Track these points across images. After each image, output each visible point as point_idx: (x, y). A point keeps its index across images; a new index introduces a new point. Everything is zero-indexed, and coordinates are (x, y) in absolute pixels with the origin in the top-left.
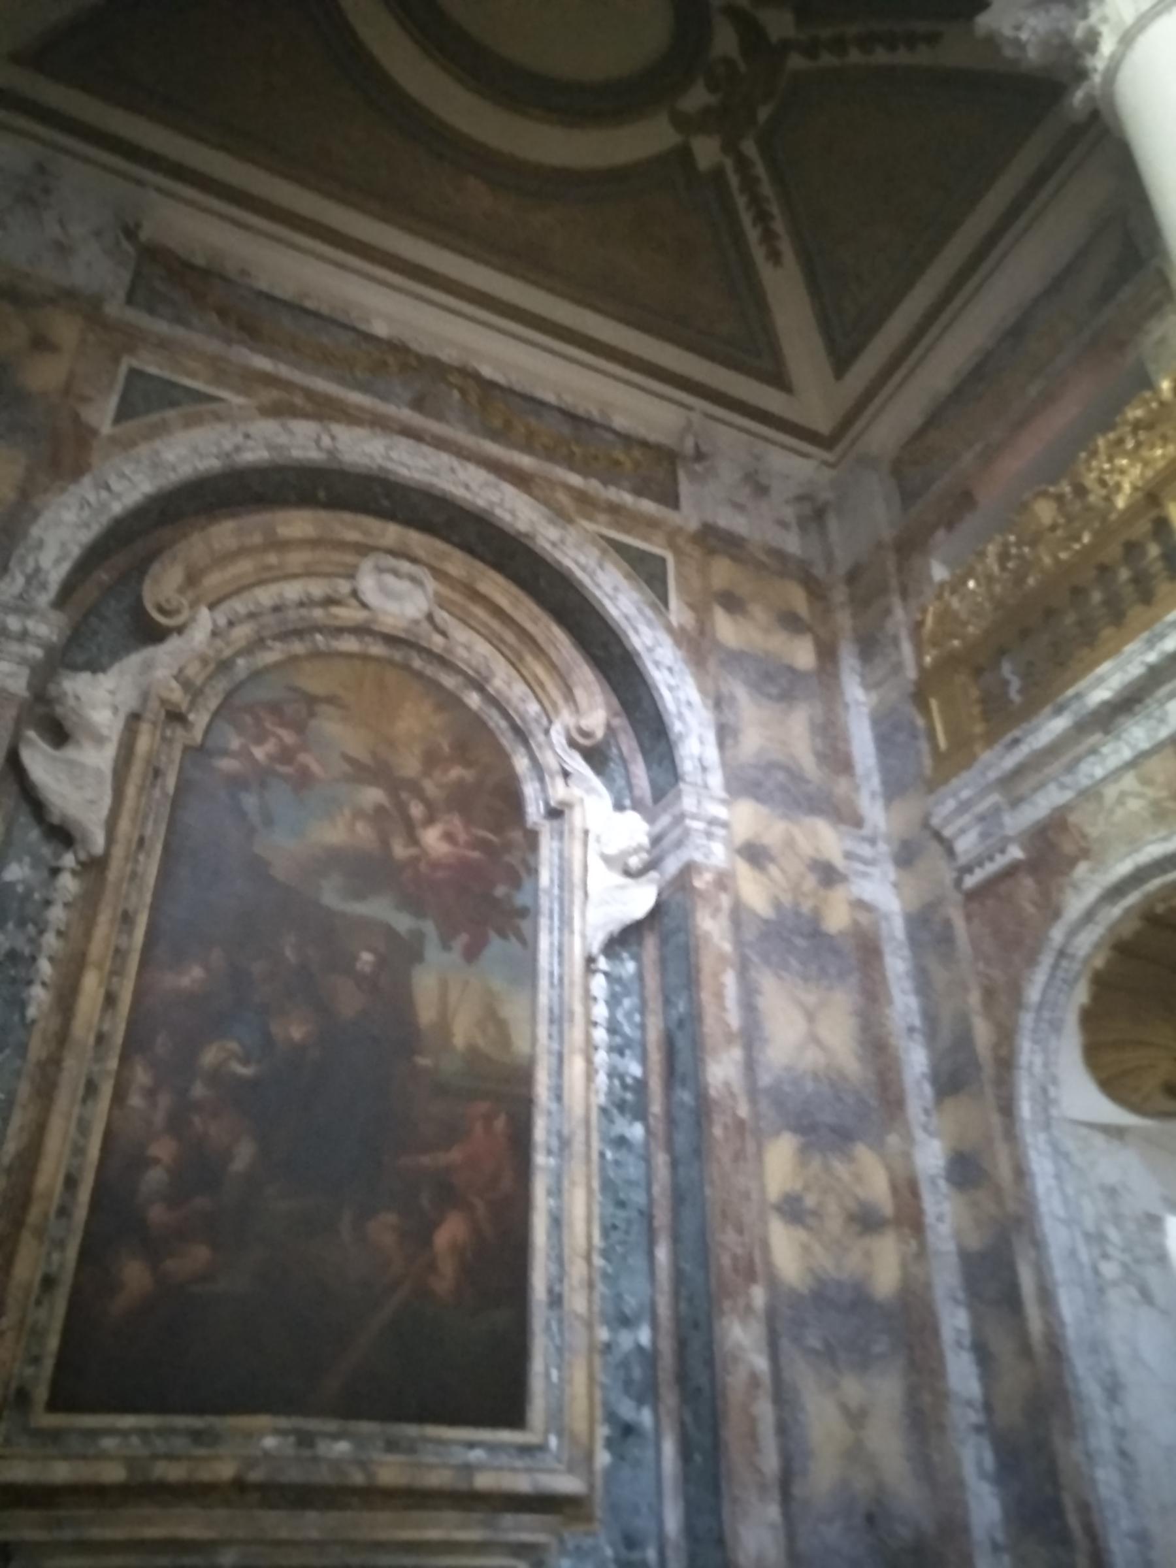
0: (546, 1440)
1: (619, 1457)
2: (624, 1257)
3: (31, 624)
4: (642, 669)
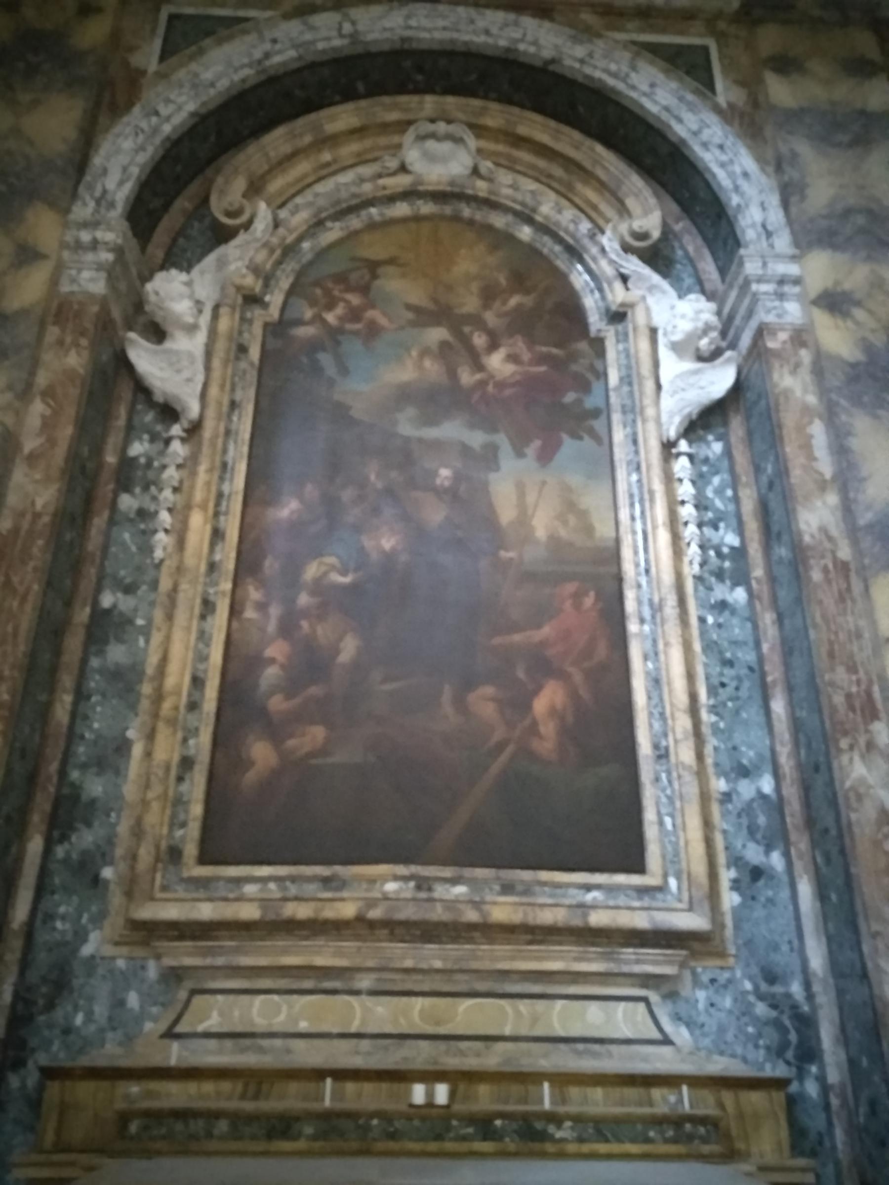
0: (666, 882)
1: (750, 898)
2: (737, 712)
3: (99, 234)
4: (692, 158)
